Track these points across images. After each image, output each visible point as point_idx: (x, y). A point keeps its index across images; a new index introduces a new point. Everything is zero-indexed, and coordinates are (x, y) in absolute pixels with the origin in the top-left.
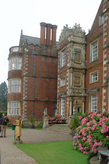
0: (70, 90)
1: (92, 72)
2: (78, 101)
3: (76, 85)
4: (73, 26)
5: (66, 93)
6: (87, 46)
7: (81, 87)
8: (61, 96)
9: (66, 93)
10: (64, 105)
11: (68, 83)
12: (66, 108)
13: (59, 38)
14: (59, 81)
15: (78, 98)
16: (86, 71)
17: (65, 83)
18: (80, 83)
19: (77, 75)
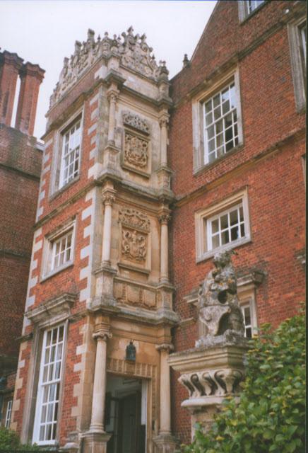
0: (99, 279)
1: (206, 208)
2: (136, 344)
3: (126, 262)
4: (121, 33)
5: (77, 297)
6: (179, 117)
7: (154, 278)
8: (46, 323)
9: (72, 300)
10: (57, 404)
11: (86, 252)
12: (70, 401)
13: (52, 93)
14: (39, 254)
15: (137, 329)
16: (173, 212)
17: (60, 351)
18: (149, 258)
19: (135, 220)
